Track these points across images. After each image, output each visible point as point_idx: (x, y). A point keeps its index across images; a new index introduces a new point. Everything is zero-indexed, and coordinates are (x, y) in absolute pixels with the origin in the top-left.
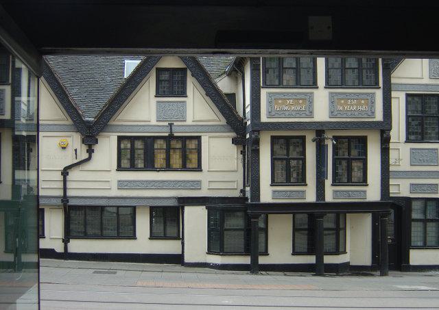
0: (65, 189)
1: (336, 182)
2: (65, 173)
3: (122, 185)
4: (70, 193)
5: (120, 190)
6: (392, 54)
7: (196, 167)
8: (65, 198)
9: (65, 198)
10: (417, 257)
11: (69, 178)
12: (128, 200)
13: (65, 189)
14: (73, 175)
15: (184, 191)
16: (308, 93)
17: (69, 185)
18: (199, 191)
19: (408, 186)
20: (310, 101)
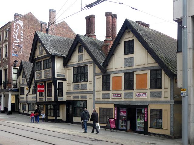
0: (27, 99)
2: (27, 95)
4: (28, 100)
5: (151, 99)
7: (92, 95)
8: (27, 101)
9: (27, 101)
11: (28, 96)
13: (27, 99)
14: (28, 96)
17: (28, 98)
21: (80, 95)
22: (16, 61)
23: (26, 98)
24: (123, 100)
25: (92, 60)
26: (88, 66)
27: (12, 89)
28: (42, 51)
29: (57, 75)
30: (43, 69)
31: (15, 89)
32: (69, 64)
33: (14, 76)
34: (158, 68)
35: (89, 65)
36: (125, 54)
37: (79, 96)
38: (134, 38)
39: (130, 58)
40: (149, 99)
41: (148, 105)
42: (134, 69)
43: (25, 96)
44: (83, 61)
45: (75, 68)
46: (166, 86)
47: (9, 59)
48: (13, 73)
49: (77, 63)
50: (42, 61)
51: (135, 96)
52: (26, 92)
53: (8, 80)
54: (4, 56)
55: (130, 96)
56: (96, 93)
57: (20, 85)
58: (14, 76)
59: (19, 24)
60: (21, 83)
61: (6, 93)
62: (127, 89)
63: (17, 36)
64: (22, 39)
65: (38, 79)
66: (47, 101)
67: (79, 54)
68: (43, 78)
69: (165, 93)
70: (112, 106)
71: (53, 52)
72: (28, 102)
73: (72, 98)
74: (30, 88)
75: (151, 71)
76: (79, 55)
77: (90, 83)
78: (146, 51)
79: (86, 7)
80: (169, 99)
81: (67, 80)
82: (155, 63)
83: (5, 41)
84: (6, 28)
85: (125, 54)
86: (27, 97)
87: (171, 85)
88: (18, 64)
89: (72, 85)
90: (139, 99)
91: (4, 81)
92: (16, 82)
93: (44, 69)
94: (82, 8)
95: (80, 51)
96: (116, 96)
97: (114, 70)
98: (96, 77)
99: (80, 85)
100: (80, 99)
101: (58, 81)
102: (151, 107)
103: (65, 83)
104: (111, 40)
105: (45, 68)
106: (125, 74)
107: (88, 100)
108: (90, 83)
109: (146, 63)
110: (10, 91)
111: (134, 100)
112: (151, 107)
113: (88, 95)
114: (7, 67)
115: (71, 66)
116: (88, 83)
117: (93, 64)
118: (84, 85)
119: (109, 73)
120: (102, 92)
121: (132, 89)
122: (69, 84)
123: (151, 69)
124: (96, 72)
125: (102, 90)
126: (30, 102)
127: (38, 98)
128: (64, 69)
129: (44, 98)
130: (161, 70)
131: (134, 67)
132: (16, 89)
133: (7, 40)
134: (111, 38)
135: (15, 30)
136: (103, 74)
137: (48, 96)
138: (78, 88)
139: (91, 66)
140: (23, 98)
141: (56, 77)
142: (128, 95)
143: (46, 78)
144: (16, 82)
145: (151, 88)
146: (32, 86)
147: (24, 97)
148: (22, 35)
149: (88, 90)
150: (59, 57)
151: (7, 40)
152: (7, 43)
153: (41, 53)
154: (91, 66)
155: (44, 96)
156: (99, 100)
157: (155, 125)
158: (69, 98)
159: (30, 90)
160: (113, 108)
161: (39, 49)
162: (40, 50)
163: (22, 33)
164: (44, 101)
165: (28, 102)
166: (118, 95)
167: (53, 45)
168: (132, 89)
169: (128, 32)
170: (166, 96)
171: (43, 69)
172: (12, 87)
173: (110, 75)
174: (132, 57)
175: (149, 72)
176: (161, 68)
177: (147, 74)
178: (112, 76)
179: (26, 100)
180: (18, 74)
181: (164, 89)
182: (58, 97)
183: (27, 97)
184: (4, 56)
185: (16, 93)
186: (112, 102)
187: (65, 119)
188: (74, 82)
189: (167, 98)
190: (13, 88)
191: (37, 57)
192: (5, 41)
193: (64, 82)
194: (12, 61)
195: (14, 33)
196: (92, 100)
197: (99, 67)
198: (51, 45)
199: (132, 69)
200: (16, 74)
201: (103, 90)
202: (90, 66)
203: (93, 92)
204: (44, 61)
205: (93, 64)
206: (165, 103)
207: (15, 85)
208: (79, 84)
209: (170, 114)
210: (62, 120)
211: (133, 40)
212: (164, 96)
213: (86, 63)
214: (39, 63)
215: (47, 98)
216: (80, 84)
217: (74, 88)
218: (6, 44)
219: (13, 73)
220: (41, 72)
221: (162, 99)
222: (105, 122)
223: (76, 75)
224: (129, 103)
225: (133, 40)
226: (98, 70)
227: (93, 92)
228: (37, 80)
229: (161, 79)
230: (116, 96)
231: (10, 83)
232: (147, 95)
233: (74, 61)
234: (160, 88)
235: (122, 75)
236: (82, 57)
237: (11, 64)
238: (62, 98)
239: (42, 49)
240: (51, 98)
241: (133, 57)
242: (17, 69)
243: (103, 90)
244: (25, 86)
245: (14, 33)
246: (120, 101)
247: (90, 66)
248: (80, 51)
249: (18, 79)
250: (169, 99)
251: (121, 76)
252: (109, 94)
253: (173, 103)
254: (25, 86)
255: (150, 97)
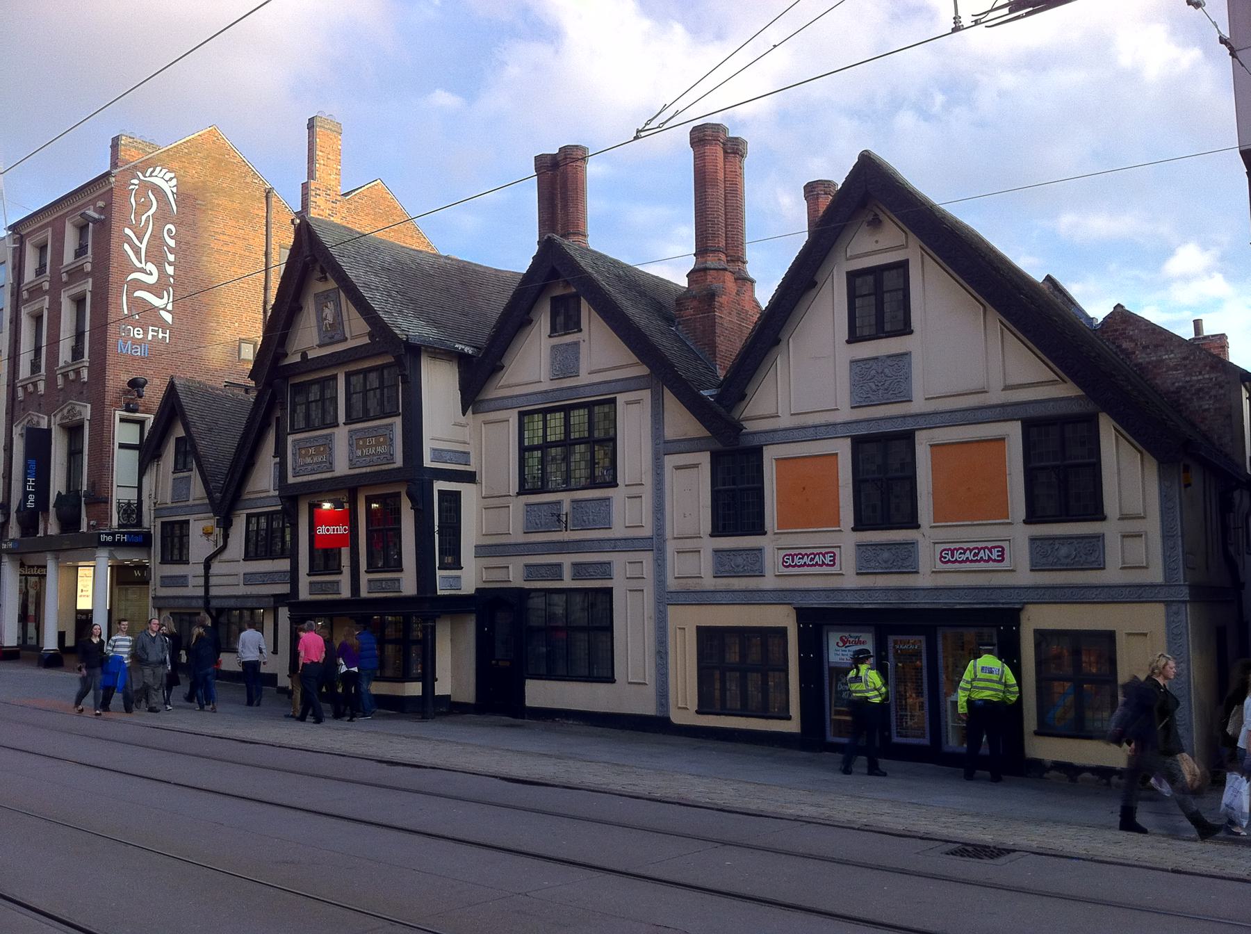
0: (207, 587)
1: (371, 568)
2: (207, 564)
3: (249, 579)
4: (214, 592)
5: (574, 582)
6: (74, 287)
7: (647, 558)
8: (207, 598)
9: (207, 598)
10: (307, 720)
11: (212, 571)
12: (114, 603)
13: (207, 587)
14: (216, 567)
15: (538, 582)
16: (327, 435)
17: (213, 581)
18: (184, 589)
19: (521, 568)
20: (328, 443)
21: (567, 560)
22: (136, 385)
23: (201, 581)
24: (851, 581)
25: (643, 370)
26: (613, 401)
27: (113, 534)
28: (338, 323)
29: (434, 450)
30: (342, 417)
31: (129, 533)
32: (494, 391)
33: (124, 465)
34: (1075, 409)
35: (621, 399)
36: (854, 337)
37: (559, 565)
38: (913, 252)
39: (889, 356)
40: (1024, 577)
41: (1020, 610)
42: (912, 416)
43: (193, 570)
44: (584, 378)
45: (531, 413)
46: (1135, 507)
47: (99, 369)
48: (122, 446)
49: (546, 385)
50: (335, 377)
51: (927, 557)
52: (199, 546)
53: (92, 485)
54: (65, 354)
55: (904, 558)
56: (671, 547)
57: (159, 511)
58: (124, 465)
59: (158, 191)
60: (167, 497)
61: (33, 559)
62: (257, 557)
63: (143, 247)
64: (170, 264)
65: (305, 479)
66: (364, 593)
67: (556, 341)
68: (342, 467)
69: (1128, 541)
70: (782, 617)
71: (410, 327)
72: (214, 603)
73: (514, 575)
74: (226, 524)
75: (1030, 426)
76: (553, 347)
77: (634, 491)
78: (995, 317)
79: (1006, 10)
80: (1156, 575)
81: (483, 477)
82: (1052, 382)
83: (76, 274)
84: (85, 205)
85: (854, 337)
86: (207, 577)
87: (1165, 498)
88: (154, 394)
89: (518, 505)
90: (963, 576)
91: (64, 493)
92: (132, 495)
93: (350, 420)
94: (957, 19)
95: (566, 321)
96: (967, 560)
97: (785, 422)
98: (670, 461)
99: (566, 508)
100: (568, 582)
101: (439, 485)
102: (1037, 618)
103: (469, 493)
104: (725, 269)
105: (354, 415)
106: (859, 443)
107: (618, 585)
108: (634, 491)
109: (996, 383)
110: (106, 544)
111: (924, 580)
112: (1037, 618)
113: (619, 562)
114: (86, 412)
115: (509, 403)
116: (617, 495)
117: (646, 395)
118: (588, 504)
119: (756, 442)
120: (710, 544)
121: (758, 528)
122: (494, 502)
123: (1032, 412)
124: (670, 433)
125: (709, 530)
126: (232, 603)
127: (304, 580)
128: (462, 419)
129: (345, 579)
130: (1090, 421)
131: (918, 405)
132: (136, 534)
133: (46, 286)
134: (723, 257)
135: (138, 215)
136: (719, 446)
137: (371, 568)
138: (557, 519)
139: (637, 402)
140: (181, 581)
141: (427, 463)
142: (886, 555)
143: (368, 470)
144: (132, 495)
145: (1032, 517)
146: (244, 517)
147: (185, 577)
148: (172, 243)
149: (618, 531)
150: (443, 353)
151: (46, 286)
152: (46, 305)
153: (332, 333)
154: (637, 402)
155: (346, 570)
156: (692, 584)
157: (1071, 715)
158: (498, 575)
159: (226, 537)
160: (782, 632)
161: (319, 312)
162: (321, 319)
163: (169, 231)
164: (346, 593)
165: (214, 603)
166: (813, 558)
167: (403, 294)
168: (758, 528)
169: (869, 224)
170: (1137, 551)
171: (342, 417)
172: (115, 523)
173: (758, 452)
174: (906, 354)
175: (1013, 432)
176: (1090, 407)
177: (1004, 439)
178: (770, 455)
179: (201, 592)
180: (149, 452)
181: (773, 537)
182: (439, 573)
183: (207, 577)
184: (65, 354)
185: (130, 557)
186: (778, 597)
187: (468, 694)
188: (522, 491)
189: (1012, 571)
190: (120, 526)
191: (304, 355)
192: (76, 274)
193: (463, 488)
194: (117, 379)
195: (127, 231)
196: (649, 587)
197: (695, 405)
198: (394, 293)
199: (904, 417)
200: (136, 453)
201: (718, 530)
202: (628, 403)
203: (654, 544)
204: (348, 376)
205: (646, 395)
206: (1136, 594)
207: (132, 512)
208: (559, 503)
209: (670, 657)
210: (449, 697)
211: (903, 266)
212: (1123, 557)
213: (603, 389)
214: (314, 393)
215: (364, 578)
216: (566, 498)
217: (528, 521)
218: (78, 290)
219: (122, 446)
220: (329, 438)
221: (1112, 575)
222: (1110, 720)
223: (538, 454)
224: (894, 601)
225: (903, 266)
226: (680, 422)
227: (654, 544)
228: (299, 479)
229: (1095, 469)
230: (967, 560)
231: (106, 501)
232: (837, 561)
233: (526, 380)
234: (1097, 514)
235: (843, 449)
236: (577, 359)
237: (109, 398)
238: (459, 577)
239: (338, 314)
240: (398, 580)
241: (906, 354)
242: (141, 423)
243: (718, 530)
244: (191, 518)
245: (127, 231)
246: (833, 590)
247: (628, 403)
248: (566, 321)
249: (146, 480)
250: (1156, 575)
251: (837, 454)
252: (760, 550)
253: (1185, 594)
254: (191, 518)
255: (1032, 565)
